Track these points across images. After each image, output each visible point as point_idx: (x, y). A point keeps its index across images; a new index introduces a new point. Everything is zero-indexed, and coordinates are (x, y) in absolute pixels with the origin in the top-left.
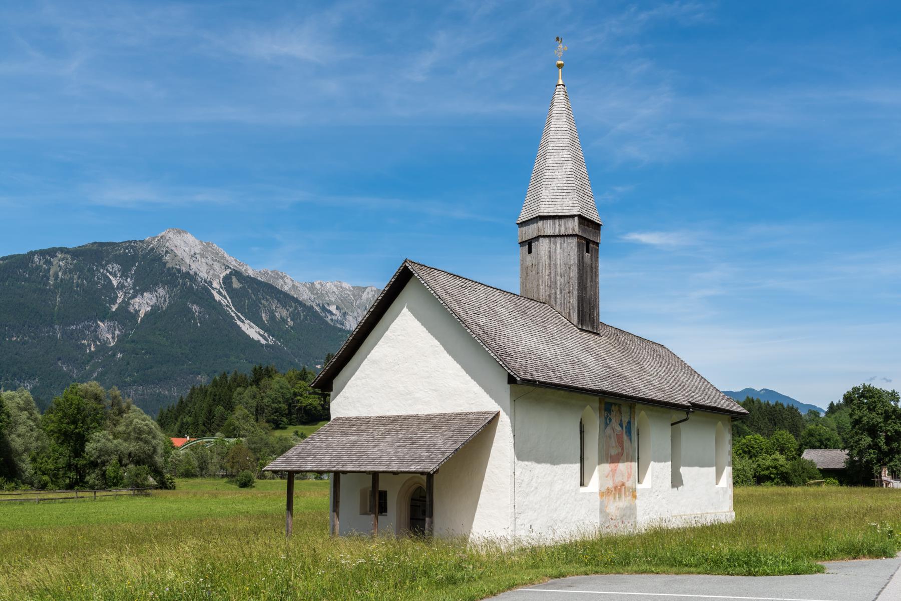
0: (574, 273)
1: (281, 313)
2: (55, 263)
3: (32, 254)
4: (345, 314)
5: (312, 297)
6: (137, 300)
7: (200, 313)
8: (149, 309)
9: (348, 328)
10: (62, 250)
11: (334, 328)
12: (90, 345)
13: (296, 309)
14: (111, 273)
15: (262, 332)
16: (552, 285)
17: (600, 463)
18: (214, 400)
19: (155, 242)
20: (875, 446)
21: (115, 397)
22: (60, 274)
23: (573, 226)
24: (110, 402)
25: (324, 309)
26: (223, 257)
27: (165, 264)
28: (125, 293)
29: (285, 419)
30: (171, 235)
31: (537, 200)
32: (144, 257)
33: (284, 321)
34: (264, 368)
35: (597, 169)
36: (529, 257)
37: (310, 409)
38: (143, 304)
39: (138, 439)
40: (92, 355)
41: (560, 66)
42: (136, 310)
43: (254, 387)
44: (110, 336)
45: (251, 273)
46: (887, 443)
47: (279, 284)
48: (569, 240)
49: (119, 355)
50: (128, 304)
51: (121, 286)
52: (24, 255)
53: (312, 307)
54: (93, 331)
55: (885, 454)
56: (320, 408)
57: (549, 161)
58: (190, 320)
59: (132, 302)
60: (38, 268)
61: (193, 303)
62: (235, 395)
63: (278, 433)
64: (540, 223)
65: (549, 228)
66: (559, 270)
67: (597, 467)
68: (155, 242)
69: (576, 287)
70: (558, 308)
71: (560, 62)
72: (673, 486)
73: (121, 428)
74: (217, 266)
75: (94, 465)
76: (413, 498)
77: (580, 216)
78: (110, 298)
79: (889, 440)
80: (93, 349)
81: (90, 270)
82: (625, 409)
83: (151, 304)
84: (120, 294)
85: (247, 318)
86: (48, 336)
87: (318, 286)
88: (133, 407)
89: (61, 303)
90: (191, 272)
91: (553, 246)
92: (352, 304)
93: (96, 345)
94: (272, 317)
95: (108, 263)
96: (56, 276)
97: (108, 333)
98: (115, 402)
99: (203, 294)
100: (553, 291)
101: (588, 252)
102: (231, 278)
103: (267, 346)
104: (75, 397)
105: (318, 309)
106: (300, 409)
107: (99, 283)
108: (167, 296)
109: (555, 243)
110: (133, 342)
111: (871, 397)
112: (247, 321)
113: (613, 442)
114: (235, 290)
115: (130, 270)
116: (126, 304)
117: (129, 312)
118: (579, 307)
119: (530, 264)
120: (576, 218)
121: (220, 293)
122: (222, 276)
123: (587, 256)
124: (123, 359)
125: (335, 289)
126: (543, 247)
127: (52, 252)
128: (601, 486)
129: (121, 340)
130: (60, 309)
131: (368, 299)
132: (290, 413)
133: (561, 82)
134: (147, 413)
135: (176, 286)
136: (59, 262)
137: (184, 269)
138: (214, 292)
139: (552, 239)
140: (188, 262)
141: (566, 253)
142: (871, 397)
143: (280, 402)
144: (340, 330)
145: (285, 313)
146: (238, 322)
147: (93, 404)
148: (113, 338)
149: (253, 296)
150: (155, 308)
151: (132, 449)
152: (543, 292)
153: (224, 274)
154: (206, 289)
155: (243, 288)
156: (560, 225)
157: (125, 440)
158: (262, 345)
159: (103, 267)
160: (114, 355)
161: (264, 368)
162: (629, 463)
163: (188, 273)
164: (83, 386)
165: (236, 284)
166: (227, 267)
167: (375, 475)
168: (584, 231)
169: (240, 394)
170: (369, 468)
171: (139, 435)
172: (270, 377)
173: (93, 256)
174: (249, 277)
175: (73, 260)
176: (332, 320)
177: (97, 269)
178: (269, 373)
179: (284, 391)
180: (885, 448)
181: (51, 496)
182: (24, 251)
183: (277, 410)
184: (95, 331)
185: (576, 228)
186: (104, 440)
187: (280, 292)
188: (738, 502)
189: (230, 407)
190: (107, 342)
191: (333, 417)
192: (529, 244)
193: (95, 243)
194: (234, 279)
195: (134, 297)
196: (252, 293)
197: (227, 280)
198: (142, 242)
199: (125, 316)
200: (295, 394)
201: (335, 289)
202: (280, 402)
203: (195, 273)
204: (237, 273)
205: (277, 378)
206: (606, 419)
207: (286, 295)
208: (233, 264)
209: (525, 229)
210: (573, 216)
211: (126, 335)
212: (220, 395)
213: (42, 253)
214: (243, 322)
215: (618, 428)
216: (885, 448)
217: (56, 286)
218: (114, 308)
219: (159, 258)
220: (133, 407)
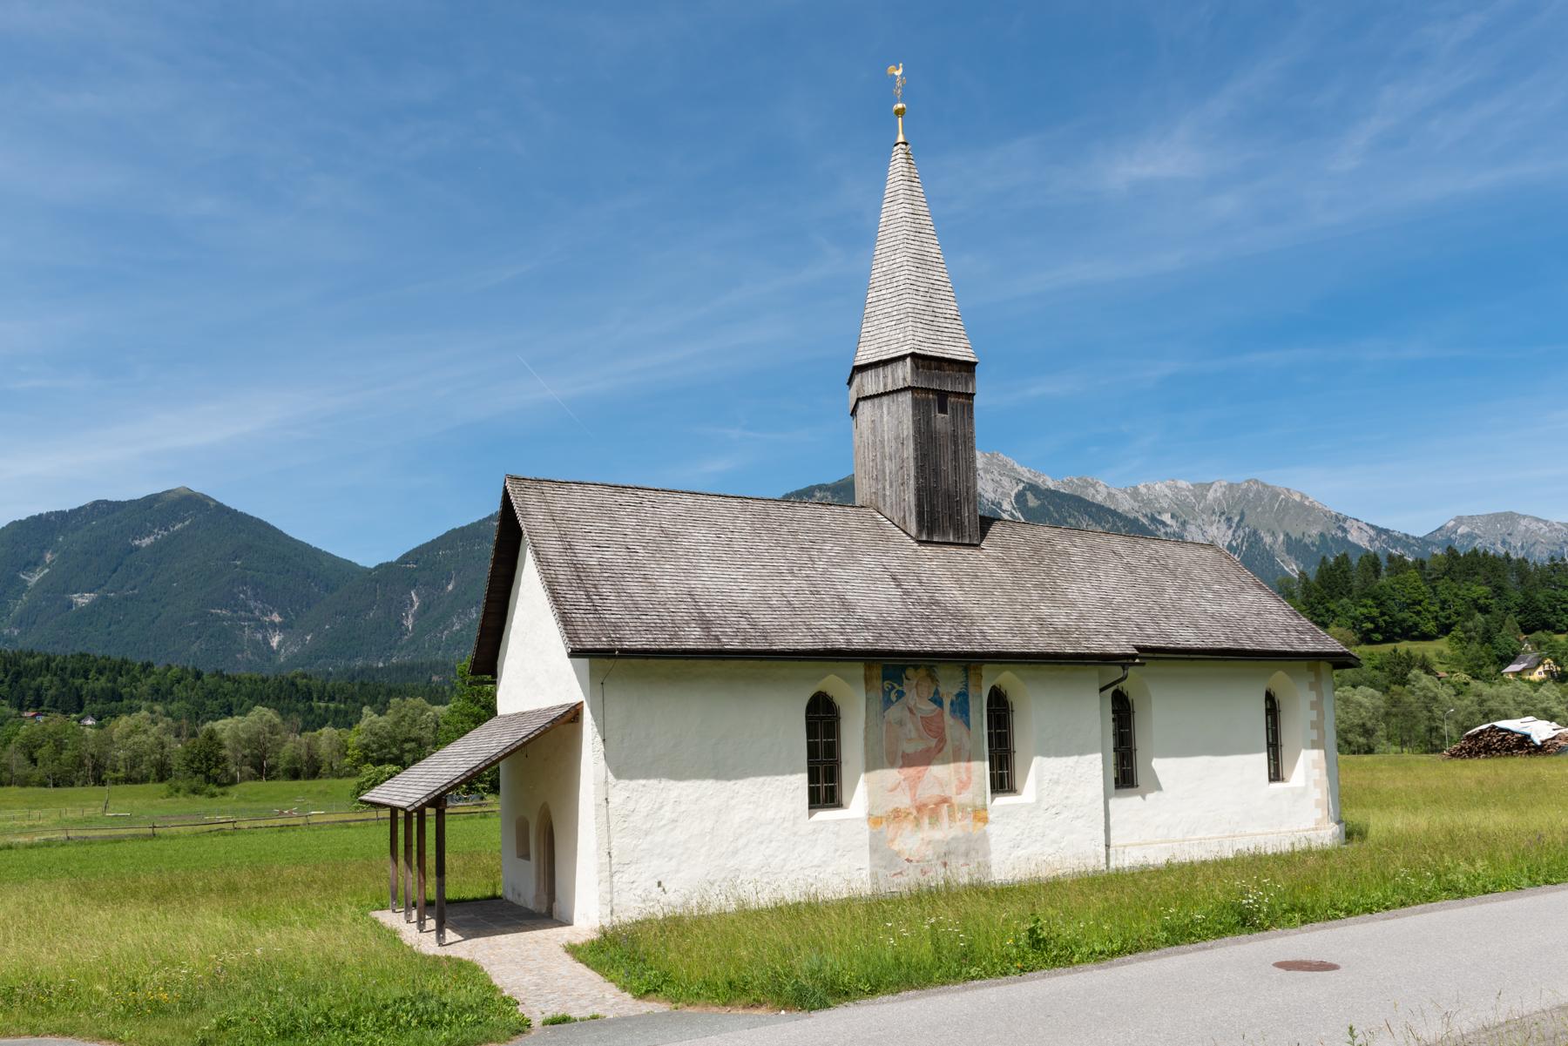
4: (1184, 523)
5: (1136, 505)
10: (821, 488)
13: (1115, 524)
17: (870, 766)
25: (1153, 519)
26: (1013, 469)
41: (899, 112)
45: (1051, 484)
47: (1089, 494)
67: (863, 776)
69: (912, 473)
71: (900, 106)
72: (1271, 780)
74: (1006, 482)
77: (913, 355)
82: (958, 673)
87: (1143, 490)
91: (878, 412)
101: (943, 410)
105: (1145, 521)
109: (881, 406)
113: (911, 729)
118: (919, 505)
120: (908, 360)
123: (941, 421)
125: (1167, 491)
128: (872, 806)
131: (1215, 500)
133: (901, 139)
139: (876, 401)
155: (1042, 505)
156: (885, 377)
162: (963, 765)
165: (1032, 502)
168: (930, 379)
174: (1049, 490)
191: (500, 713)
194: (1029, 496)
197: (1020, 497)
201: (1167, 491)
204: (1032, 488)
206: (886, 694)
207: (1100, 507)
208: (1026, 474)
210: (903, 358)
215: (928, 708)
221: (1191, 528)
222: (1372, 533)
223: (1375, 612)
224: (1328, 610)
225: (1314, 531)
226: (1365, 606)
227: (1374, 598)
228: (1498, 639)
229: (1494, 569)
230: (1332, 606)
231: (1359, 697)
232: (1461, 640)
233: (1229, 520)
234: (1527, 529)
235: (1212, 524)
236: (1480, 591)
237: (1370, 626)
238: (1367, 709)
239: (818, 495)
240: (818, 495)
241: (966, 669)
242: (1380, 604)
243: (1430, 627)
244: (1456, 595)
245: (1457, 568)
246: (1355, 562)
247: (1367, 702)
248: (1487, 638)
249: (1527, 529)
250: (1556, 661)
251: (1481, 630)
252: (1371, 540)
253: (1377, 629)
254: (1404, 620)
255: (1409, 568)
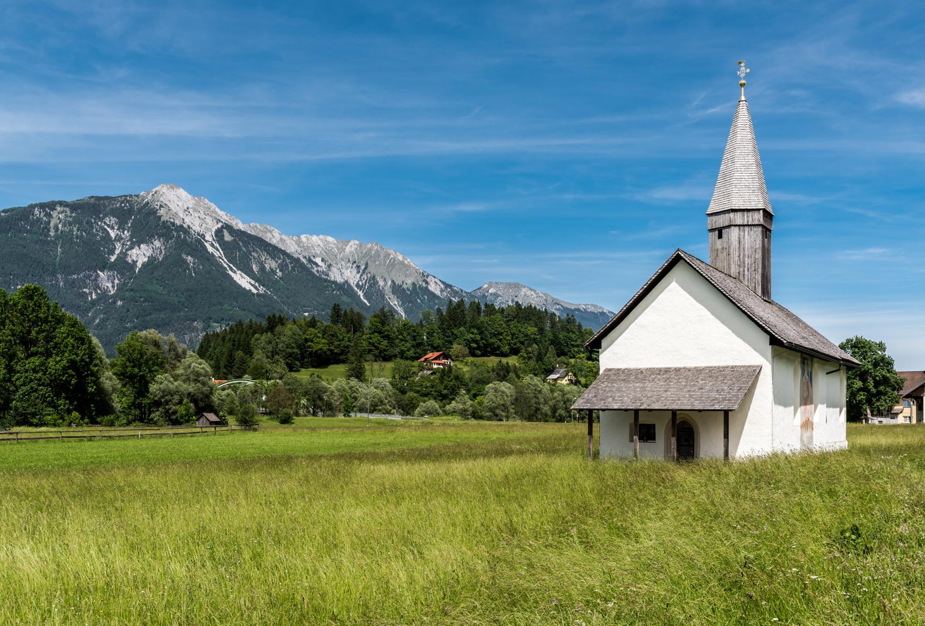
0: (759, 255)
1: (271, 264)
2: (54, 216)
3: (32, 207)
4: (330, 266)
5: (299, 250)
6: (134, 251)
7: (194, 264)
8: (146, 259)
9: (333, 279)
10: (61, 203)
11: (320, 279)
12: (91, 293)
13: (284, 260)
14: (108, 226)
15: (253, 282)
16: (741, 264)
18: (234, 345)
19: (150, 197)
20: (865, 389)
21: (172, 343)
22: (60, 226)
23: (759, 218)
24: (167, 347)
25: (310, 261)
26: (215, 212)
27: (160, 217)
28: (123, 244)
29: (298, 363)
30: (165, 190)
31: (728, 195)
32: (140, 210)
33: (273, 272)
34: (277, 316)
35: (773, 173)
36: (719, 242)
37: (321, 354)
38: (140, 255)
39: (196, 381)
40: (94, 303)
41: (742, 85)
42: (133, 261)
43: (269, 334)
44: (110, 285)
45: (241, 226)
46: (875, 387)
48: (755, 229)
49: (119, 303)
50: (126, 255)
51: (119, 238)
52: (25, 208)
53: (298, 259)
54: (93, 281)
55: (874, 395)
56: (328, 353)
57: (737, 165)
58: (185, 271)
59: (129, 253)
60: (39, 219)
61: (188, 255)
62: (253, 340)
63: (294, 374)
64: (732, 215)
65: (738, 219)
66: (746, 253)
68: (150, 197)
70: (746, 283)
73: (180, 371)
74: (209, 220)
75: (157, 404)
76: (680, 431)
77: (764, 210)
78: (108, 249)
79: (877, 384)
80: (94, 297)
81: (89, 222)
83: (148, 255)
84: (118, 246)
85: (239, 269)
86: (52, 285)
88: (190, 353)
89: (62, 253)
90: (185, 226)
91: (742, 233)
92: (336, 256)
93: (97, 294)
94: (262, 269)
95: (106, 216)
96: (57, 229)
97: (108, 282)
98: (172, 348)
99: (196, 246)
100: (741, 269)
102: (222, 231)
103: (258, 295)
104: (137, 344)
106: (311, 353)
107: (97, 235)
108: (163, 248)
109: (744, 231)
110: (132, 290)
111: (862, 347)
112: (239, 272)
114: (227, 242)
115: (127, 223)
116: (124, 255)
117: (127, 263)
119: (720, 247)
121: (212, 245)
122: (214, 230)
124: (123, 306)
126: (734, 233)
127: (52, 205)
129: (121, 288)
130: (61, 259)
131: (351, 252)
132: (303, 358)
134: (202, 358)
135: (171, 239)
136: (58, 216)
137: (178, 222)
138: (207, 245)
140: (182, 216)
141: (753, 238)
142: (862, 347)
143: (293, 348)
144: (326, 280)
145: (274, 265)
146: (230, 273)
147: (152, 349)
148: (113, 287)
149: (244, 249)
150: (152, 260)
151: (191, 390)
152: (734, 271)
153: (216, 227)
154: (199, 241)
155: (234, 240)
157: (184, 382)
158: (253, 294)
159: (101, 220)
160: (115, 302)
161: (277, 316)
163: (182, 226)
164: (143, 333)
165: (228, 237)
166: (219, 221)
167: (637, 412)
169: (257, 340)
170: (632, 407)
171: (197, 377)
172: (283, 324)
173: (91, 209)
174: (239, 230)
175: (71, 212)
176: (318, 271)
177: (95, 222)
178: (281, 321)
179: (297, 337)
180: (874, 390)
181: (181, 431)
182: (25, 204)
183: (290, 355)
184: (96, 280)
185: (762, 219)
186: (166, 382)
187: (270, 245)
188: (849, 433)
189: (249, 352)
190: (106, 291)
192: (720, 232)
193: (92, 197)
194: (226, 232)
195: (131, 248)
196: (242, 246)
197: (219, 233)
198: (137, 196)
199: (123, 267)
200: (306, 340)
202: (293, 348)
203: (189, 227)
205: (289, 326)
207: (275, 248)
208: (224, 216)
209: (714, 218)
210: (759, 210)
211: (125, 284)
212: (239, 340)
213: (42, 206)
214: (235, 272)
216: (874, 390)
217: (57, 237)
218: (113, 258)
219: (154, 212)
220: (190, 353)
221: (334, 269)
222: (442, 286)
223: (478, 337)
224: (453, 334)
225: (409, 281)
226: (473, 333)
227: (478, 329)
228: (545, 359)
229: (540, 318)
230: (455, 332)
231: (503, 388)
232: (525, 358)
233: (358, 267)
234: (525, 295)
235: (347, 269)
236: (532, 330)
237: (475, 345)
238: (507, 396)
239: (59, 209)
240: (59, 209)
241: (803, 363)
242: (481, 333)
243: (506, 349)
244: (520, 331)
245: (521, 315)
246: (467, 306)
247: (508, 392)
248: (540, 358)
249: (525, 295)
250: (575, 375)
251: (536, 353)
252: (442, 291)
253: (478, 348)
254: (493, 344)
255: (497, 312)
